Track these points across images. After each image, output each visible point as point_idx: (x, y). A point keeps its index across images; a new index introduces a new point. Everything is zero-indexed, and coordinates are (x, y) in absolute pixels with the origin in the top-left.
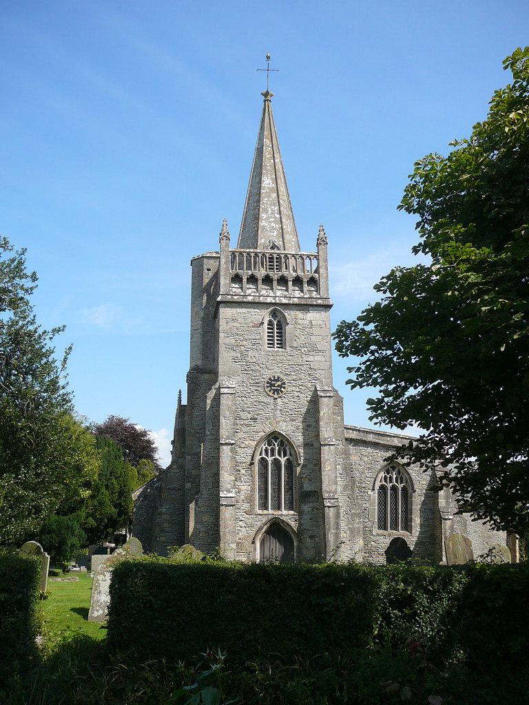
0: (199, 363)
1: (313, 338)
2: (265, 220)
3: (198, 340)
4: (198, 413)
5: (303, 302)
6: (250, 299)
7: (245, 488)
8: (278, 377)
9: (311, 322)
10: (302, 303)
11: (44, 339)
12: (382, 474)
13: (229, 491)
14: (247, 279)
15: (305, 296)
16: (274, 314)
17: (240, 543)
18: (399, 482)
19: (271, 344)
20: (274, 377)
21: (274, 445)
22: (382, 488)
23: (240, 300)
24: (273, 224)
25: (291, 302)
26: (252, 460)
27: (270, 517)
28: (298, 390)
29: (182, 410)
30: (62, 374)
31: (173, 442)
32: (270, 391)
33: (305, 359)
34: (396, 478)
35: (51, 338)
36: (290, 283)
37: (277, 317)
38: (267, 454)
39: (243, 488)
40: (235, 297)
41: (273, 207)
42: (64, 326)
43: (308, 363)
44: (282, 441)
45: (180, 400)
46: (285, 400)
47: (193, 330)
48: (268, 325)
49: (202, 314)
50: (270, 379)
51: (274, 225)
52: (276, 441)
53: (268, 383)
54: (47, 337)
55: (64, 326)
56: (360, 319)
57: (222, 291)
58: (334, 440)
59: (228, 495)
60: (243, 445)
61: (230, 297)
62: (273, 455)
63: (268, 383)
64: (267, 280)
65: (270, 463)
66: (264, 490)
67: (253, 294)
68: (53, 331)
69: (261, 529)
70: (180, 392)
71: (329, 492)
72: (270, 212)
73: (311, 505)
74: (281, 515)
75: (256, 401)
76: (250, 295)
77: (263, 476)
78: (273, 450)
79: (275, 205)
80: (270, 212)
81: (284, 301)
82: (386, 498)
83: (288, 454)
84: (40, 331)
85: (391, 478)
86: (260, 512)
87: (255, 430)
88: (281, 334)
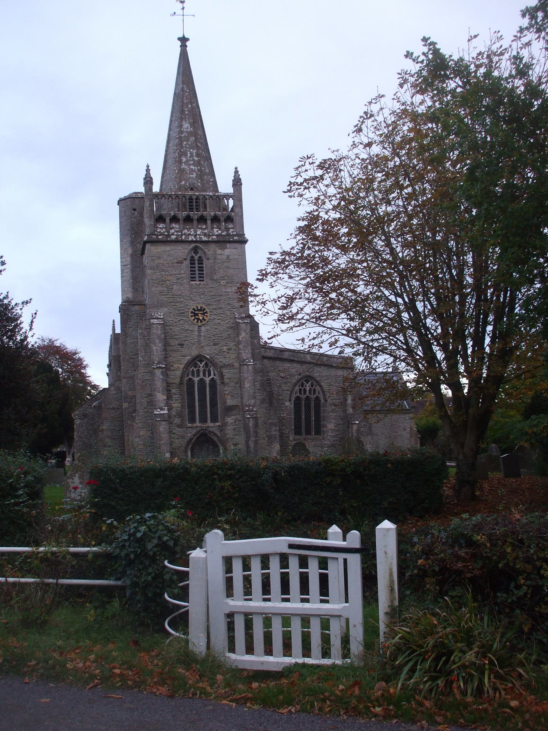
0: (130, 295)
1: (231, 271)
2: (184, 163)
3: (128, 275)
4: (131, 341)
5: (221, 239)
6: (173, 237)
7: (176, 405)
8: (201, 307)
9: (228, 257)
10: (221, 240)
11: (16, 310)
12: (297, 388)
13: (162, 409)
14: (170, 220)
15: (223, 234)
16: (196, 250)
17: (173, 452)
18: (312, 394)
19: (193, 279)
20: (197, 307)
21: (200, 367)
22: (298, 398)
23: (165, 239)
24: (192, 167)
25: (210, 239)
26: (181, 380)
27: (198, 429)
28: (219, 318)
29: (115, 338)
30: (30, 334)
31: (109, 366)
32: (194, 320)
33: (224, 290)
34: (310, 390)
35: (21, 309)
36: (209, 222)
37: (198, 253)
38: (193, 375)
39: (175, 405)
40: (160, 237)
41: (191, 150)
42: (31, 299)
43: (226, 293)
44: (206, 363)
45: (114, 329)
46: (208, 327)
47: (123, 266)
48: (190, 260)
49: (130, 251)
50: (194, 309)
51: (193, 167)
52: (201, 363)
53: (192, 312)
54: (18, 308)
55: (31, 299)
56: (518, 32)
57: (148, 231)
58: (252, 360)
59: (162, 412)
60: (172, 368)
61: (155, 237)
62: (198, 375)
63: (192, 312)
64: (188, 220)
65: (196, 382)
66: (191, 406)
67: (175, 234)
68: (23, 303)
69: (191, 439)
70: (114, 321)
71: (249, 406)
72: (189, 155)
73: (233, 417)
74: (208, 427)
75: (183, 329)
76: (173, 234)
77: (191, 393)
78: (198, 371)
79: (193, 149)
80: (189, 155)
81: (204, 239)
82: (310, 410)
83: (212, 374)
84: (13, 303)
85: (305, 390)
86: (190, 425)
87: (182, 355)
88: (201, 269)
